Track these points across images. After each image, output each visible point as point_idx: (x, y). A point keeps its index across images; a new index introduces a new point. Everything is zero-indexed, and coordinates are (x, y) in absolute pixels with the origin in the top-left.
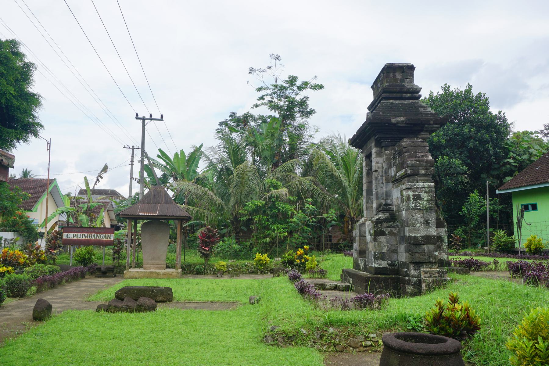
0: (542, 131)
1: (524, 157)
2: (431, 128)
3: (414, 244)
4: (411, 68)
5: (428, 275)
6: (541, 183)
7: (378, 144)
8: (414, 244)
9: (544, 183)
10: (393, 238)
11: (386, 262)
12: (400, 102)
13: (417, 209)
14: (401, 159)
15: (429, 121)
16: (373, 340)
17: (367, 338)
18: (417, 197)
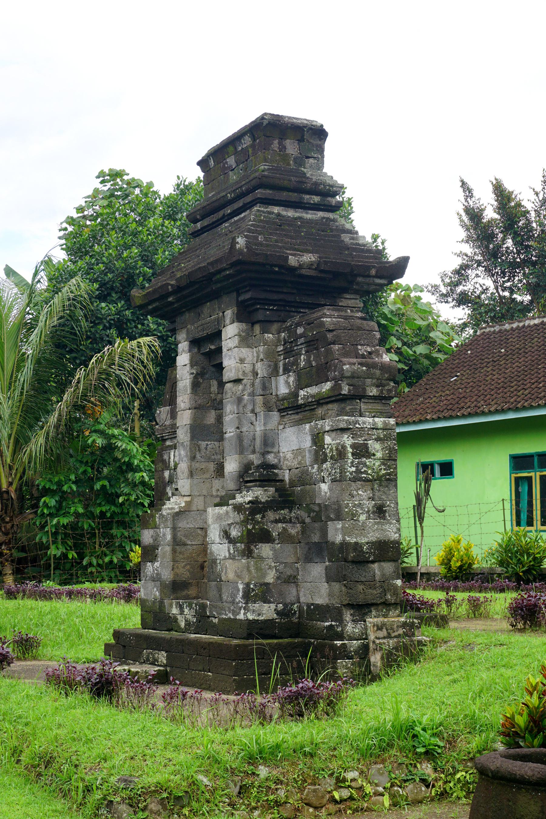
0: (436, 287)
1: (421, 349)
2: (368, 284)
3: (353, 562)
4: (320, 133)
5: (384, 633)
6: (470, 415)
7: (245, 315)
8: (353, 562)
9: (476, 414)
10: (289, 548)
11: (273, 606)
12: (297, 215)
13: (360, 479)
14: (317, 357)
15: (369, 268)
16: (353, 784)
17: (340, 782)
18: (362, 451)
